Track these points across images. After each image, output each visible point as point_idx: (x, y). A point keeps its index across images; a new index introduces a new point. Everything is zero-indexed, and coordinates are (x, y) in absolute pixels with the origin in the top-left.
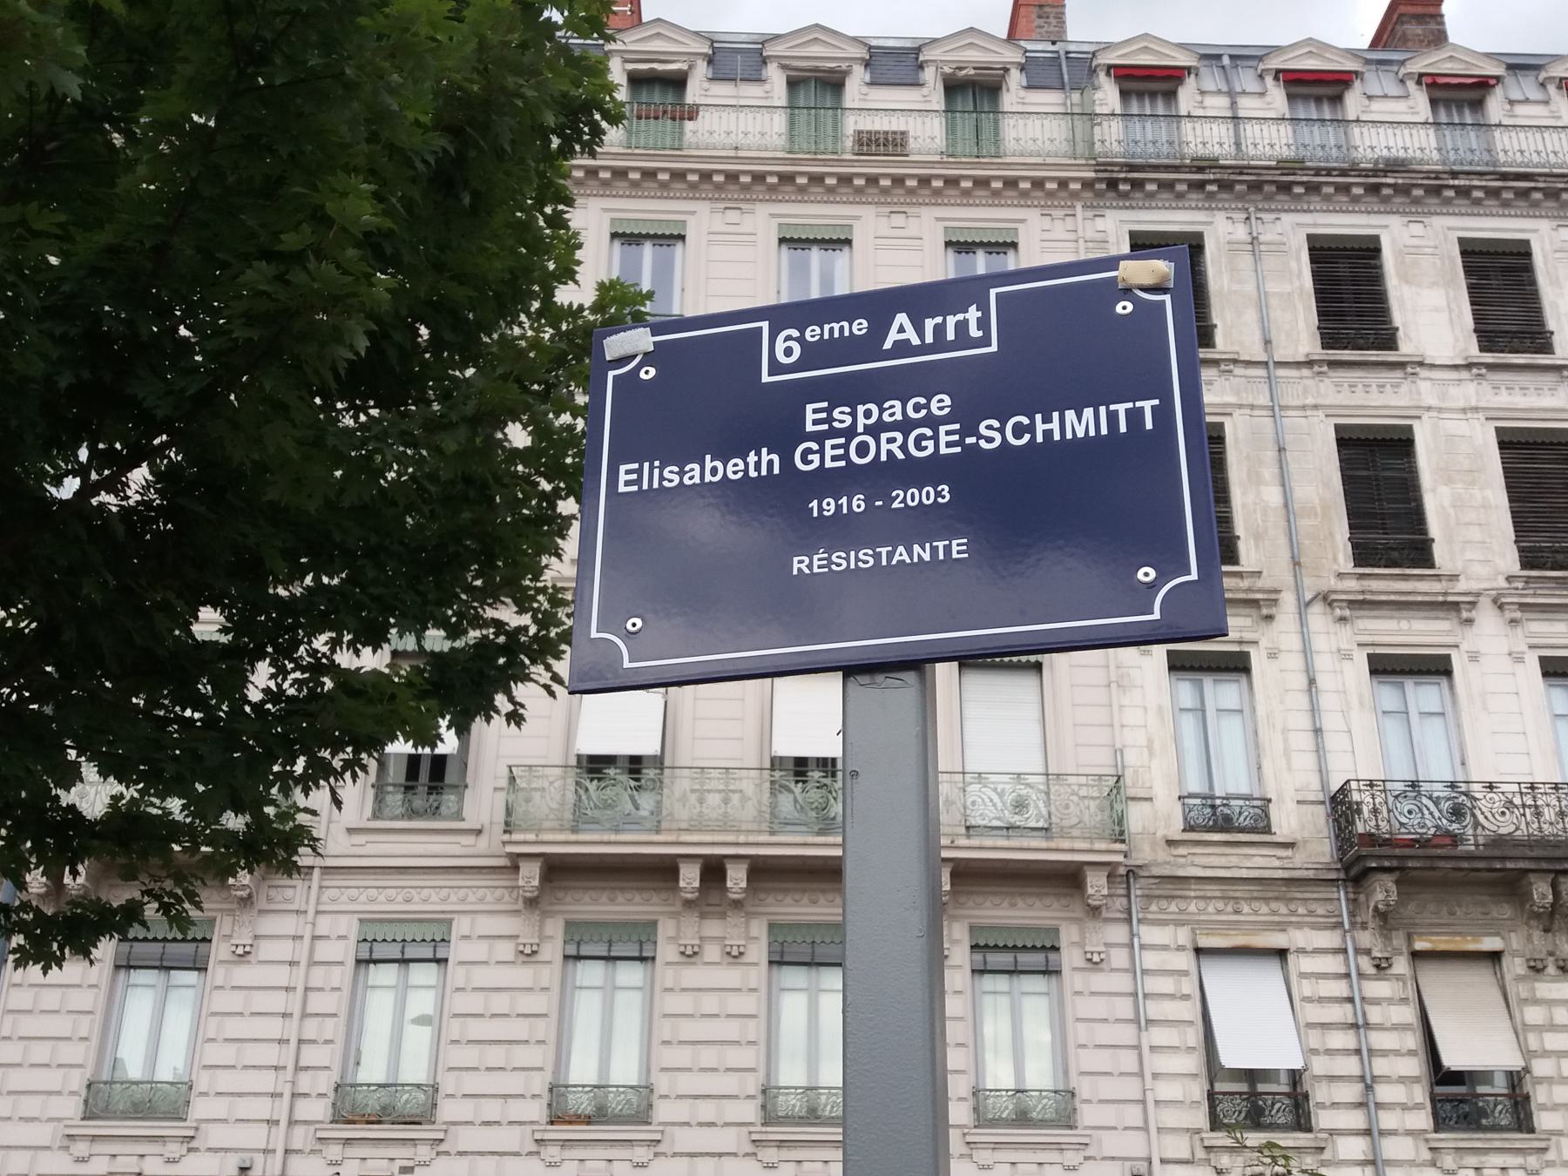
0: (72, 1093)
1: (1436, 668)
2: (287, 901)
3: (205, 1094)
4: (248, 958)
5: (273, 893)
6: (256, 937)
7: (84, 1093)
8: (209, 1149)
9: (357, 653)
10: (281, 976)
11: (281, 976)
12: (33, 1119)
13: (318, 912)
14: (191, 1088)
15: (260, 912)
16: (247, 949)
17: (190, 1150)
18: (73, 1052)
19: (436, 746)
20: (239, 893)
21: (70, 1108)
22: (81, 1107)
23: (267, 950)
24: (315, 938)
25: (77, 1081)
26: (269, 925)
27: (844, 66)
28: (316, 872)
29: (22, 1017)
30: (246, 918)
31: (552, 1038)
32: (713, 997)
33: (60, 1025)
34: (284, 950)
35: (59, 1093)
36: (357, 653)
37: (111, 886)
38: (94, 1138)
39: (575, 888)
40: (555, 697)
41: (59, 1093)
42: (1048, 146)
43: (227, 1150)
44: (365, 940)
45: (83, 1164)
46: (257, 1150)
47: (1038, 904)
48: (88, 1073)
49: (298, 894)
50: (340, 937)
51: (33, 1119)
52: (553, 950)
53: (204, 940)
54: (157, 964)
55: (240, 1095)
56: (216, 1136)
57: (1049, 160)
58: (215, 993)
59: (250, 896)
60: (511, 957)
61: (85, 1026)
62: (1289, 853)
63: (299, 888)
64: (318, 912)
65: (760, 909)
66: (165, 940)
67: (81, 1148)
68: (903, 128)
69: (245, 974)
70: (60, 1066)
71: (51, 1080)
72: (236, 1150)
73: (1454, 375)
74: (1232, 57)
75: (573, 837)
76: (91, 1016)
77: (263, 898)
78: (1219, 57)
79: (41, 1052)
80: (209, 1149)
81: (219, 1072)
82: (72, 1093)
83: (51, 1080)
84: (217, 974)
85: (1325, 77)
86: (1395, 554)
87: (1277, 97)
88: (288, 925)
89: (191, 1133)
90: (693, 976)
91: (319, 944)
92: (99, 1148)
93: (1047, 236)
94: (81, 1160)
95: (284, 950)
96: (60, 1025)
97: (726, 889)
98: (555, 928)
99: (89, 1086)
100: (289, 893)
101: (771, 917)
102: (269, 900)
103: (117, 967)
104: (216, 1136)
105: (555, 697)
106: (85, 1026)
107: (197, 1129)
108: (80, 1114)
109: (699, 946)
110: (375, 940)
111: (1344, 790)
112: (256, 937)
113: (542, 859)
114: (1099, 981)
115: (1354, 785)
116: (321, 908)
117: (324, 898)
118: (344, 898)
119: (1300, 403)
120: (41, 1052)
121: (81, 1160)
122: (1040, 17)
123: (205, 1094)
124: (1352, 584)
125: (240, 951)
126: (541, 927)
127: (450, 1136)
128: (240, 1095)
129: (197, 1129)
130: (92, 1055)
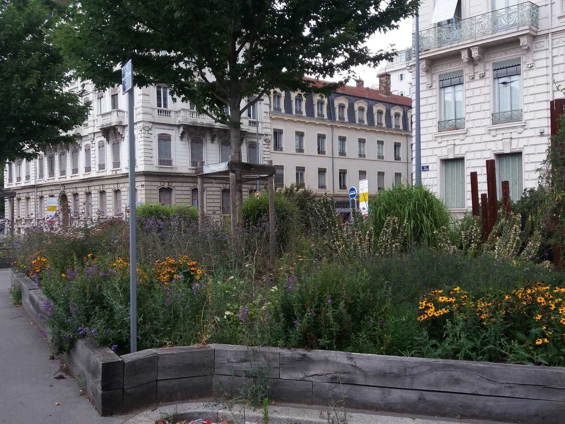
0: (435, 126)
2: (542, 46)
3: (527, 112)
4: (533, 68)
5: (537, 45)
6: (534, 61)
7: (491, 117)
8: (530, 128)
9: (242, 57)
10: (544, 71)
11: (544, 71)
12: (479, 127)
13: (553, 48)
14: (522, 111)
15: (534, 52)
16: (532, 65)
17: (524, 129)
18: (486, 106)
19: (357, 46)
20: (524, 48)
21: (489, 122)
22: (492, 122)
23: (538, 64)
24: (553, 57)
25: (489, 114)
26: (538, 56)
28: (550, 35)
29: (471, 99)
30: (529, 55)
31: (438, 109)
32: (478, 90)
33: (481, 99)
34: (544, 63)
35: (485, 118)
36: (242, 57)
37: (488, 54)
38: (496, 130)
39: (493, 53)
41: (485, 118)
43: (536, 128)
44: (441, 80)
45: (521, 134)
46: (545, 127)
47: (508, 53)
48: (492, 111)
49: (545, 44)
50: (562, 55)
51: (479, 127)
52: (436, 85)
53: (518, 65)
54: (506, 75)
55: (537, 111)
56: (531, 124)
58: (524, 81)
59: (529, 48)
60: (469, 80)
61: (488, 98)
63: (545, 42)
64: (553, 48)
65: (490, 60)
66: (506, 67)
67: (493, 133)
69: (532, 73)
70: (483, 111)
71: (482, 115)
72: (538, 127)
75: (439, 49)
76: (489, 95)
77: (534, 48)
79: (477, 108)
80: (530, 128)
81: (530, 105)
82: (435, 126)
83: (482, 115)
84: (524, 75)
88: (543, 54)
89: (524, 124)
90: (473, 85)
91: (555, 59)
92: (498, 132)
94: (494, 136)
95: (544, 63)
96: (481, 99)
97: (462, 60)
98: (436, 78)
99: (492, 115)
100: (542, 44)
101: (492, 62)
102: (536, 48)
103: (495, 79)
104: (531, 124)
106: (488, 98)
107: (525, 123)
108: (492, 124)
109: (484, 73)
110: (443, 80)
112: (534, 61)
113: (467, 49)
116: (554, 46)
117: (554, 43)
118: (561, 41)
120: (477, 108)
121: (494, 136)
123: (527, 112)
125: (529, 66)
126: (474, 70)
127: (526, 124)
128: (537, 111)
129: (525, 123)
130: (438, 115)
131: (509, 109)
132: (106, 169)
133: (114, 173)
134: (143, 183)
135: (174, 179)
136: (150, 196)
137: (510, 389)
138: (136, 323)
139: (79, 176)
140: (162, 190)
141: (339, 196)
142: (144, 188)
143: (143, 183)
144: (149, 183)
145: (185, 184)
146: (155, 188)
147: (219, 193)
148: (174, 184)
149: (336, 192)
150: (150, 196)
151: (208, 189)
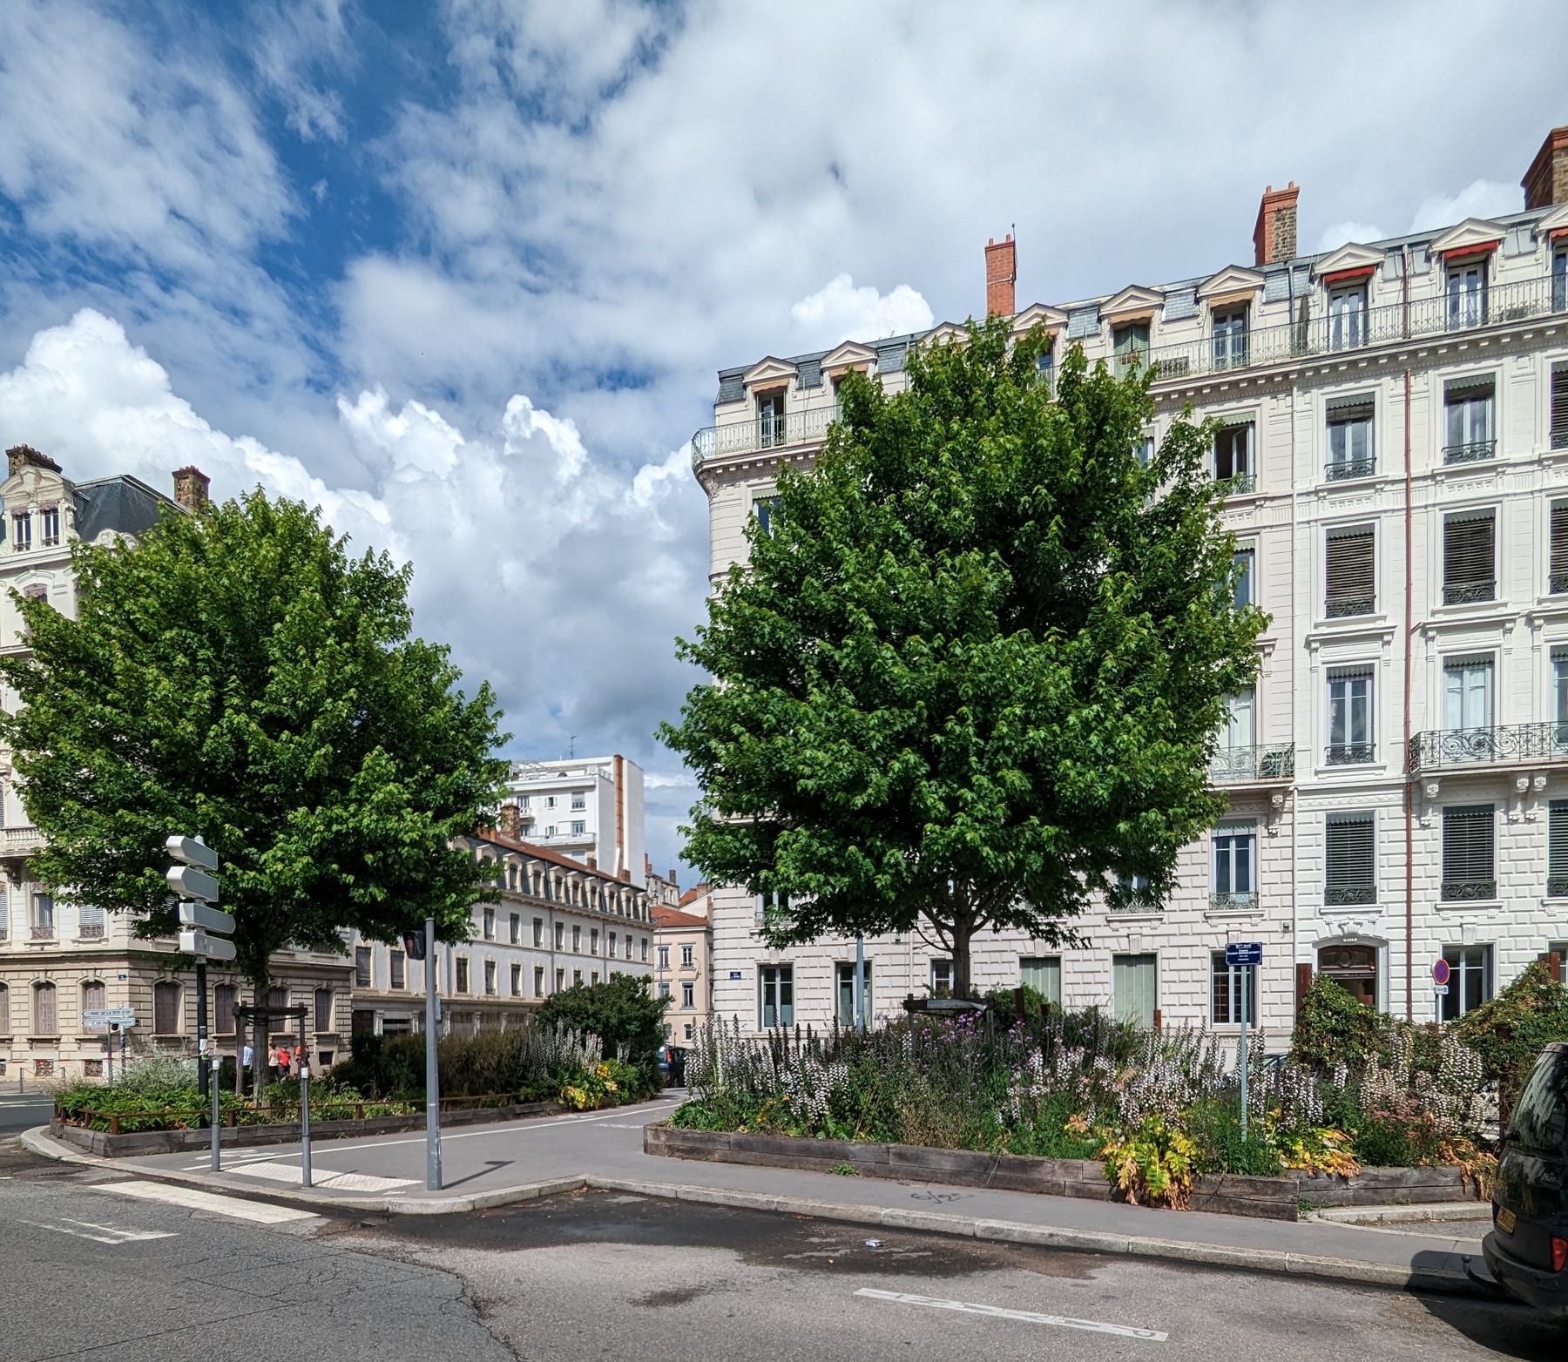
1: (1484, 662)
27: (1146, 314)
40: (371, 548)
42: (1278, 352)
57: (1278, 361)
62: (1381, 771)
68: (1381, 897)
73: (1531, 468)
74: (1410, 245)
78: (1400, 248)
85: (1475, 249)
86: (1470, 594)
87: (1437, 272)
93: (1274, 412)
105: (371, 548)
111: (1417, 737)
114: (1274, 842)
115: (1422, 735)
119: (1423, 504)
122: (1278, 220)
124: (1441, 617)
131: (60, 910)
132: (8, 940)
133: (37, 948)
134: (126, 972)
135: (290, 973)
136: (137, 998)
137: (225, 328)
138: (675, 1162)
139: (10, 944)
140: (38, 986)
141: (456, 1002)
142: (127, 982)
143: (126, 972)
144: (135, 973)
145: (306, 982)
146: (73, 982)
147: (310, 996)
148: (290, 981)
149: (453, 997)
150: (137, 998)
151: (294, 988)
